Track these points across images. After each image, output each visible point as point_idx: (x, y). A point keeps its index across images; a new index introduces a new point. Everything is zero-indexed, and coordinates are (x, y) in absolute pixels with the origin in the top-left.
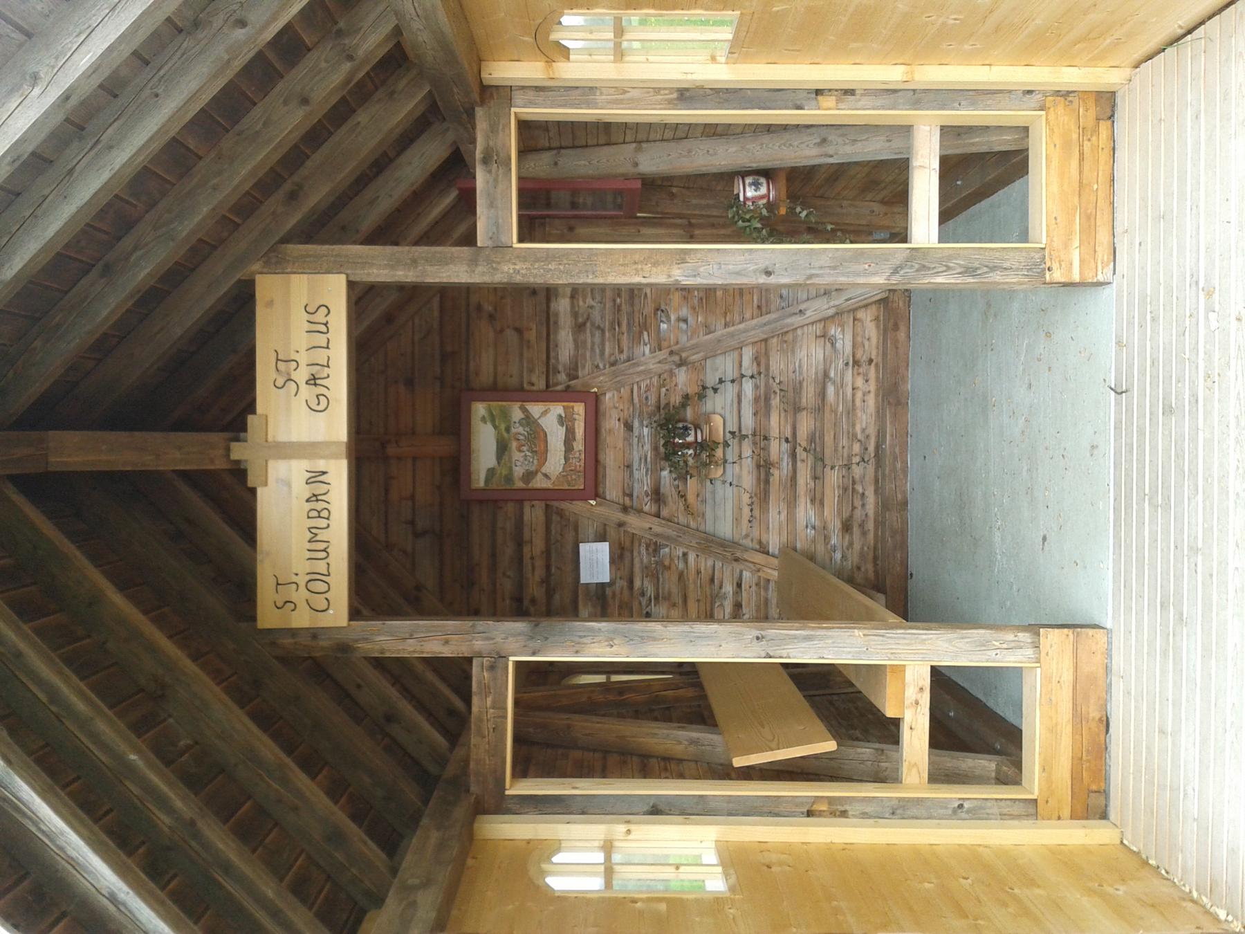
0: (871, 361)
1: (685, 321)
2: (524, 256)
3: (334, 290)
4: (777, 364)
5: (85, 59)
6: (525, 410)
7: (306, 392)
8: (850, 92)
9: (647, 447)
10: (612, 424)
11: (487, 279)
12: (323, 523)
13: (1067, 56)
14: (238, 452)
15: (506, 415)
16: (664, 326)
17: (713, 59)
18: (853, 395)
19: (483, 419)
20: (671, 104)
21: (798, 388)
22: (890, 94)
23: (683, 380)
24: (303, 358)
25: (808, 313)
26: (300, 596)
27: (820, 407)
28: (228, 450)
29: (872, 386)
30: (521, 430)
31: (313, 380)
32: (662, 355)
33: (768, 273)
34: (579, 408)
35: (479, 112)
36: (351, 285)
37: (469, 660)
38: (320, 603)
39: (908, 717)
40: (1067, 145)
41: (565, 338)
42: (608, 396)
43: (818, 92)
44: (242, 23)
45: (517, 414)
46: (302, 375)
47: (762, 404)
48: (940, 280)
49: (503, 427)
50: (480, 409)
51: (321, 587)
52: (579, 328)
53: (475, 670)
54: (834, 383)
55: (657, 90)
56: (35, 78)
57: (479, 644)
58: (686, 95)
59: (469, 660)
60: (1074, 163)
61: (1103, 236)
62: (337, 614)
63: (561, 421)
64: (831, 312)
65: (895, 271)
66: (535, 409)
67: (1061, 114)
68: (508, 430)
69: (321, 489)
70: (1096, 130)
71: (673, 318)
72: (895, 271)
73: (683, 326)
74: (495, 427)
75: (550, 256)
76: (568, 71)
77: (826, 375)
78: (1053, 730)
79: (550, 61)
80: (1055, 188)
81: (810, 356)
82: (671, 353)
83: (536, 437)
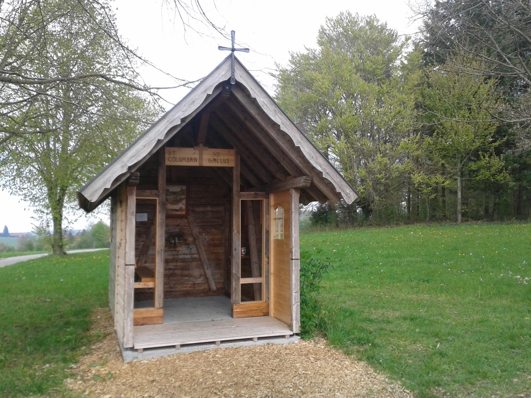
0: (194, 288)
1: (205, 240)
2: (238, 201)
3: (232, 164)
4: (194, 264)
5: (280, 143)
6: (184, 199)
7: (213, 158)
8: (268, 263)
9: (173, 231)
10: (179, 221)
11: (234, 194)
12: (186, 161)
13: (276, 302)
14: (201, 145)
15: (183, 194)
16: (204, 234)
17: (274, 237)
18: (186, 284)
19: (182, 188)
20: (266, 229)
21: (188, 269)
22: (268, 271)
23: (190, 239)
24: (219, 158)
25: (207, 271)
26: (172, 156)
27: (182, 276)
28: (201, 143)
29: (188, 289)
30: (179, 198)
31: (215, 160)
32: (198, 234)
33: (235, 249)
34: (184, 213)
35: (264, 193)
36: (232, 168)
37: (157, 190)
38: (170, 159)
39: (142, 283)
40: (259, 307)
41: (201, 209)
42: (186, 220)
43: (268, 257)
44: (283, 160)
45: (183, 197)
46: (216, 157)
47: (184, 260)
48: (234, 283)
49: (180, 193)
50: (184, 188)
51: (174, 160)
52: (203, 212)
53: (155, 191)
54: (189, 279)
55: (269, 227)
56: (278, 136)
57: (161, 191)
58: (268, 233)
59: (157, 190)
60: (256, 309)
61: (242, 315)
62: (168, 163)
63: (181, 208)
64: (208, 276)
65: (235, 274)
66: (184, 202)
67: (265, 305)
68: (179, 195)
69: (193, 160)
70: (262, 312)
71: (206, 236)
72: (235, 274)
73: (204, 239)
74: (180, 192)
75: (238, 206)
76: (272, 210)
77: (191, 277)
78: (141, 313)
79: (274, 206)
80: (251, 305)
81: (196, 272)
82: (198, 236)
83: (177, 202)
